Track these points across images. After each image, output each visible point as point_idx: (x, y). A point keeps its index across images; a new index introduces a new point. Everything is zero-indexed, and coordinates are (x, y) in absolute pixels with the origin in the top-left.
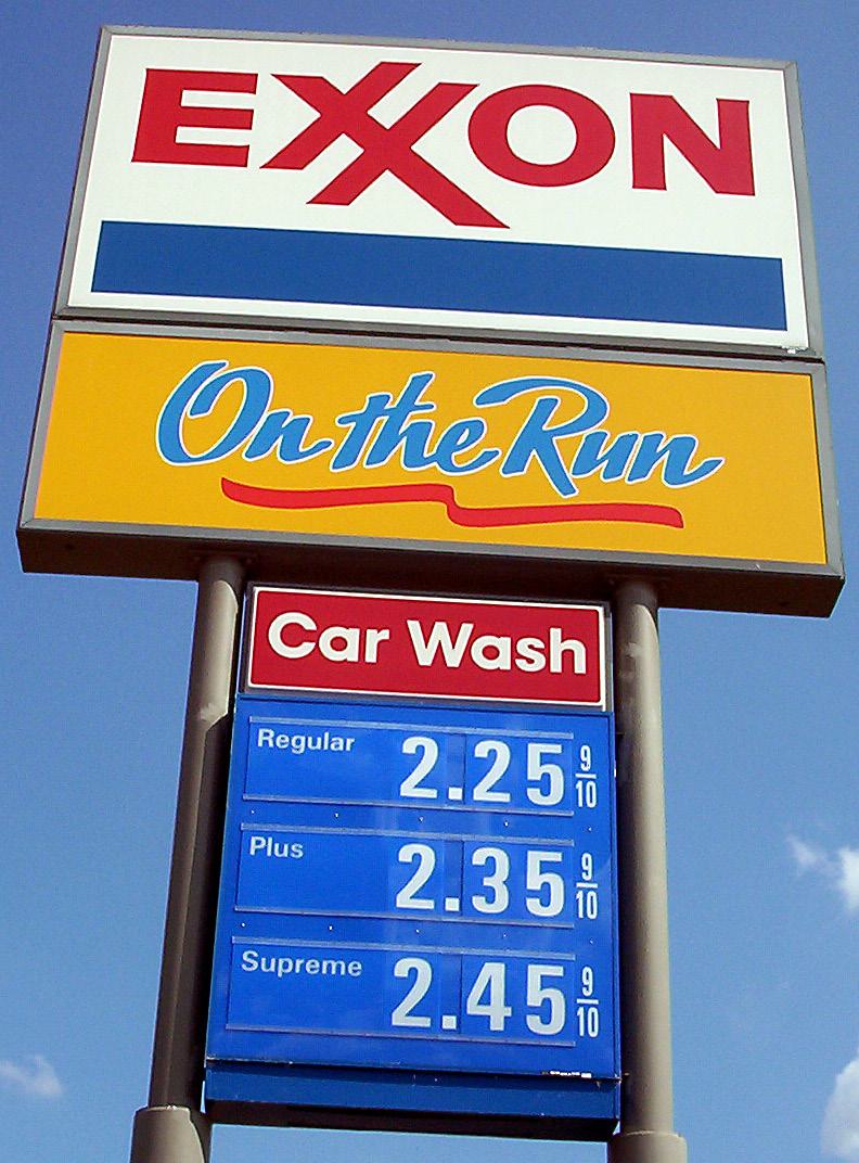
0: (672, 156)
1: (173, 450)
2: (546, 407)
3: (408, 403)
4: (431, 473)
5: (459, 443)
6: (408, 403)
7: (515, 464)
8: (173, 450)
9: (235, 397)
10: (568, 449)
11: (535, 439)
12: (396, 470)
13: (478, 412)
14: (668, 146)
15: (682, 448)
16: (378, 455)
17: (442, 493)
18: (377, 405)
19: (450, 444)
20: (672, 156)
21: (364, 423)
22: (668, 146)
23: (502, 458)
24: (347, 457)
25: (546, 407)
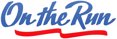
0: (77, 22)
1: (5, 24)
2: (80, 8)
3: (52, 9)
4: (57, 26)
5: (109, 21)
6: (52, 9)
7: (73, 23)
8: (5, 24)
9: (15, 9)
10: (84, 18)
11: (78, 16)
12: (49, 26)
13: (65, 11)
14: (77, 20)
15: (108, 15)
16: (45, 23)
17: (58, 31)
18: (45, 9)
19: (60, 19)
20: (77, 22)
21: (42, 14)
22: (77, 20)
23: (70, 22)
24: (39, 24)
25: (80, 8)
